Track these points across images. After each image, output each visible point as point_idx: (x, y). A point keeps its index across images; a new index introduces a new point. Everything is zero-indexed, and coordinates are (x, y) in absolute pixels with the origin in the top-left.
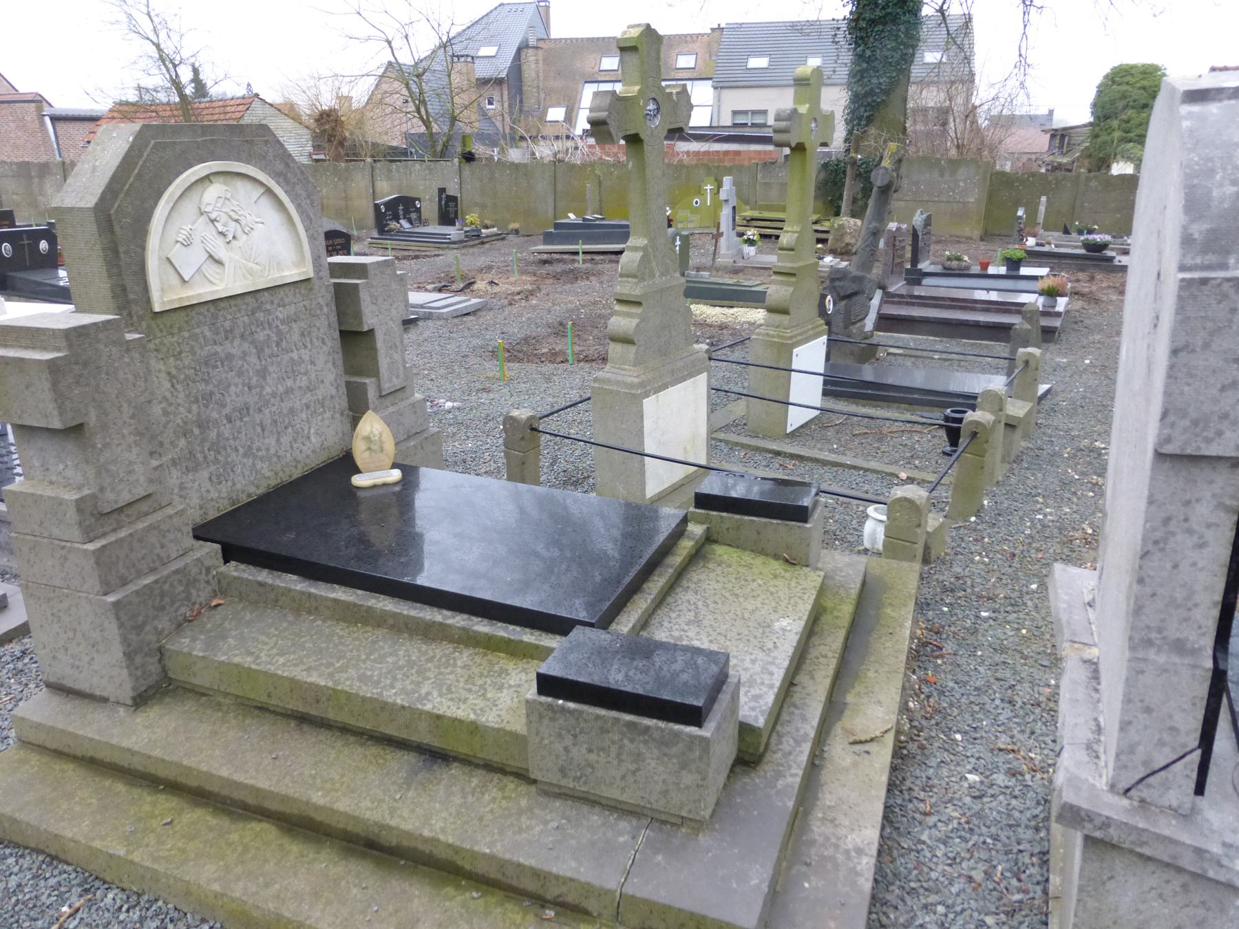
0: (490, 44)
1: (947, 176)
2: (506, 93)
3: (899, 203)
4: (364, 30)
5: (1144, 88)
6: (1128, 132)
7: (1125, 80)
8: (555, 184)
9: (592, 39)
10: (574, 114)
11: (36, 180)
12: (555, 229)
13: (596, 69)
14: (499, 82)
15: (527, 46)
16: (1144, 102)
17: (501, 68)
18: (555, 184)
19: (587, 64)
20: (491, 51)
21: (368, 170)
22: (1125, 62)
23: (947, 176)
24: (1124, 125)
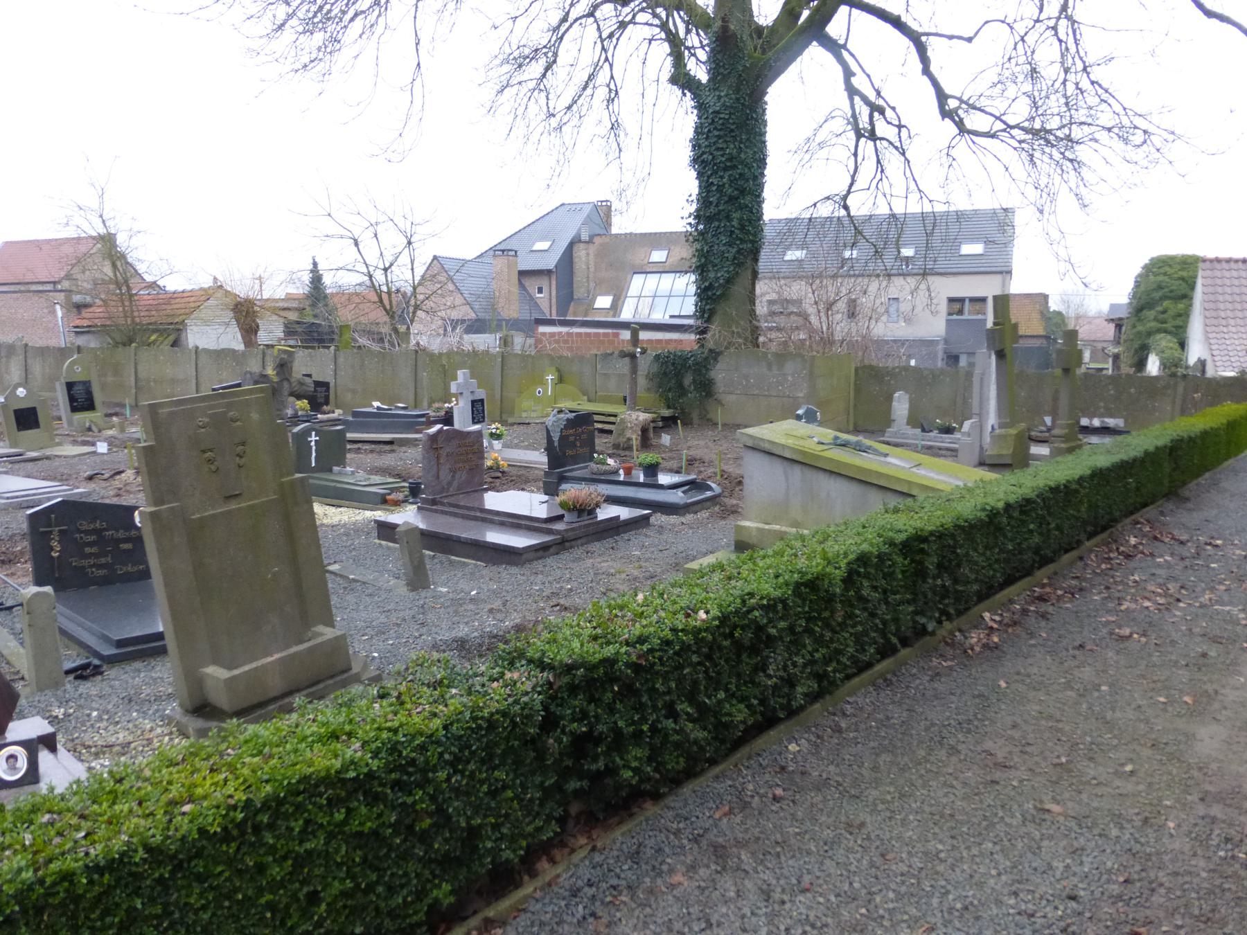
0: (543, 239)
1: (775, 371)
2: (554, 282)
3: (731, 396)
4: (336, 230)
5: (1183, 279)
6: (1165, 322)
7: (1162, 271)
8: (416, 372)
9: (645, 234)
10: (621, 302)
11: (4, 360)
12: (353, 417)
13: (646, 261)
14: (549, 272)
15: (580, 241)
16: (1183, 292)
17: (550, 262)
18: (416, 372)
19: (638, 257)
20: (544, 245)
21: (260, 356)
22: (1163, 253)
23: (775, 371)
24: (1161, 316)
